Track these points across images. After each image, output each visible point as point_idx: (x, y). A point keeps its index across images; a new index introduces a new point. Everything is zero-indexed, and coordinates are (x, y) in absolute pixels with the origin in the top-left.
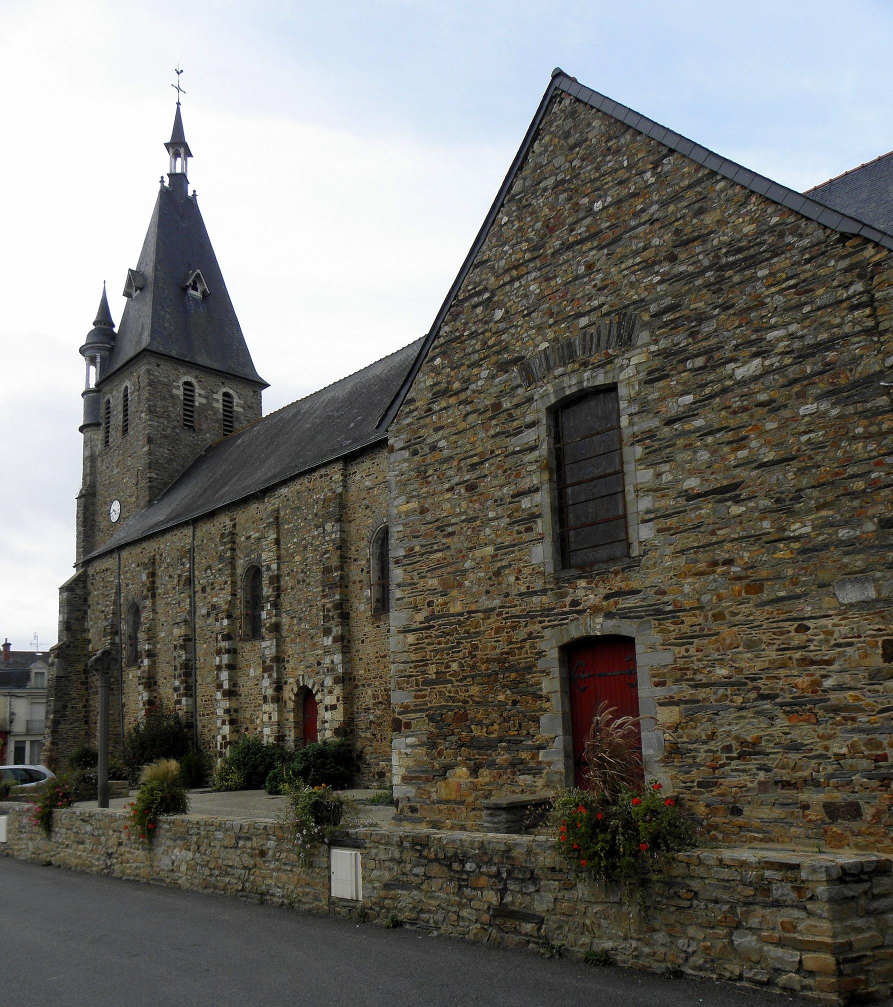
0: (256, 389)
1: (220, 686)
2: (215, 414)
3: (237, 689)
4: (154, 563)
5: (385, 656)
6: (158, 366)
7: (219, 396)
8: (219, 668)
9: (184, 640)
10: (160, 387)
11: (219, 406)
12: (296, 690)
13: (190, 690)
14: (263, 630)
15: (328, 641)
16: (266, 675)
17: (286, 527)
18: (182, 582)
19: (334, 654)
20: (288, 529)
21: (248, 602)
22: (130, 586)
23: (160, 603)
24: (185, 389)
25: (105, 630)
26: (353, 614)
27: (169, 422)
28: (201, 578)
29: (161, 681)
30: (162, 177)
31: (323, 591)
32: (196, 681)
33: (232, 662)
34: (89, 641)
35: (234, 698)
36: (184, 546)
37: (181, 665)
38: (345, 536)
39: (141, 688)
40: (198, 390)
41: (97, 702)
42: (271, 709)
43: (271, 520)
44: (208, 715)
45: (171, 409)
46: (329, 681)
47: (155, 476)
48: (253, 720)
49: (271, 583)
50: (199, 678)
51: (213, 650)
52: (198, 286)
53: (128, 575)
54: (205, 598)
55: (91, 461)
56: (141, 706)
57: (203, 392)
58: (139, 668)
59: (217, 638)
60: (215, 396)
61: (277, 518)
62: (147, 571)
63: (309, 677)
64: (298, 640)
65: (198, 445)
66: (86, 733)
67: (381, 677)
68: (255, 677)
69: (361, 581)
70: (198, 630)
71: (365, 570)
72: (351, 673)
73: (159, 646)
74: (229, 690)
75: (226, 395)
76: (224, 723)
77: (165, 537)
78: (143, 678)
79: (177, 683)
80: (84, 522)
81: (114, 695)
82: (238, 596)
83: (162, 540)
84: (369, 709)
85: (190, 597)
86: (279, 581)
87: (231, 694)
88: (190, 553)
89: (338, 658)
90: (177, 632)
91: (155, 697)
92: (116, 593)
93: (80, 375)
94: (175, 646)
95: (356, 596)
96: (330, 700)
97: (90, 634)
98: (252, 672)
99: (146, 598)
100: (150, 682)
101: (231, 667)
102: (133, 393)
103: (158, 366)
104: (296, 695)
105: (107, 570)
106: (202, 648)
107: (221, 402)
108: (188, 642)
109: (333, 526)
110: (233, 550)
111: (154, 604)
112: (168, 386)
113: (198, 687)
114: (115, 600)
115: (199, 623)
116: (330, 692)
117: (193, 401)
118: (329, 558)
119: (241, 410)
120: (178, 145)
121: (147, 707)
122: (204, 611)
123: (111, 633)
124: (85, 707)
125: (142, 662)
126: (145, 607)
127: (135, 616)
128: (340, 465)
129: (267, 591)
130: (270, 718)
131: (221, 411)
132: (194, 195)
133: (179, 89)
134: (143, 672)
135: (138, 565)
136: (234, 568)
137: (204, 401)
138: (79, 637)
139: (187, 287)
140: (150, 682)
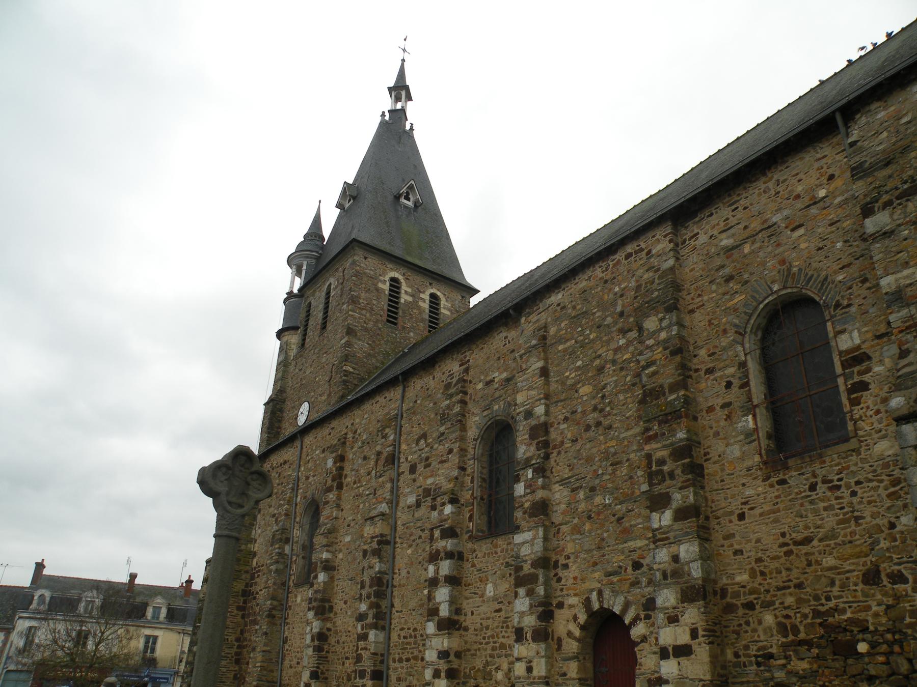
0: (464, 294)
1: (433, 612)
2: (420, 313)
3: (462, 618)
4: (344, 443)
5: (807, 541)
6: (366, 258)
7: (426, 296)
8: (433, 583)
9: (379, 543)
10: (365, 279)
11: (426, 306)
12: (582, 618)
13: (381, 619)
14: (518, 514)
15: (666, 518)
16: (522, 591)
17: (561, 347)
18: (381, 463)
19: (678, 542)
20: (565, 350)
21: (484, 480)
22: (311, 479)
23: (347, 495)
24: (391, 285)
25: (274, 536)
26: (710, 468)
27: (371, 315)
28: (409, 453)
29: (339, 605)
30: (384, 112)
31: (647, 430)
32: (392, 606)
33: (455, 573)
34: (254, 554)
35: (456, 633)
36: (388, 413)
37: (372, 579)
38: (684, 333)
39: (311, 615)
40: (404, 287)
41: (257, 640)
42: (532, 654)
43: (534, 342)
44: (408, 660)
45: (375, 302)
46: (667, 597)
47: (351, 370)
48: (490, 673)
49: (532, 437)
50: (397, 602)
51: (426, 555)
52: (410, 196)
53: (310, 465)
54: (414, 480)
55: (283, 365)
56: (308, 640)
57: (409, 290)
58: (312, 585)
59: (432, 536)
60: (422, 295)
61: (544, 338)
62: (334, 455)
63: (615, 593)
64: (587, 527)
65: (400, 343)
66: (235, 677)
67: (799, 586)
68: (495, 599)
69: (728, 405)
70: (400, 528)
71: (736, 382)
72: (715, 582)
73: (340, 556)
74: (449, 619)
75: (433, 296)
76: (437, 674)
77: (362, 408)
78: (316, 600)
79: (363, 607)
80: (268, 428)
81: (275, 624)
82: (469, 471)
83: (357, 412)
84: (771, 656)
85: (392, 480)
86: (547, 432)
87: (449, 625)
88: (395, 421)
89: (688, 550)
90: (369, 530)
91: (329, 630)
92: (293, 489)
93: (286, 281)
94: (365, 553)
95: (717, 434)
96: (669, 636)
97: (257, 545)
98: (490, 590)
99: (329, 490)
100: (323, 607)
101: (453, 581)
102: (336, 287)
103: (366, 258)
104: (583, 628)
105: (285, 462)
106: (405, 554)
107: (428, 302)
108: (384, 545)
109: (661, 320)
110: (463, 402)
111: (339, 498)
112: (374, 279)
113: (395, 615)
114: (290, 497)
115: (403, 517)
116: (673, 620)
117: (398, 298)
118: (654, 373)
119: (448, 313)
120: (400, 90)
121: (316, 643)
122: (411, 500)
123: (281, 540)
124: (238, 640)
125: (316, 577)
126: (327, 503)
127: (313, 517)
128: (668, 228)
129: (524, 450)
130: (529, 669)
131: (427, 311)
132: (412, 129)
133: (404, 50)
134: (316, 592)
135: (323, 451)
136: (464, 429)
137: (410, 299)
138: (243, 547)
139: (400, 195)
140: (323, 607)
